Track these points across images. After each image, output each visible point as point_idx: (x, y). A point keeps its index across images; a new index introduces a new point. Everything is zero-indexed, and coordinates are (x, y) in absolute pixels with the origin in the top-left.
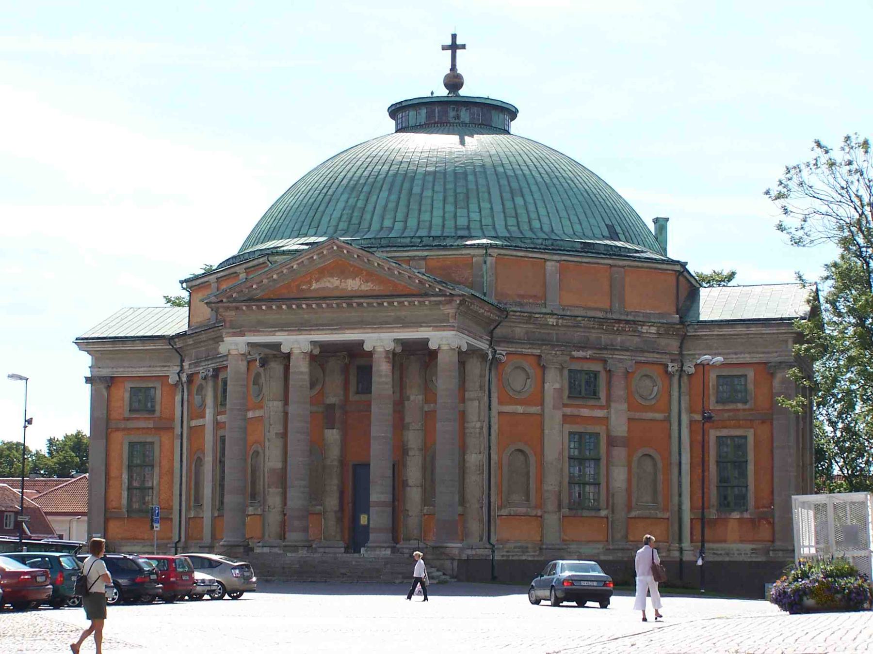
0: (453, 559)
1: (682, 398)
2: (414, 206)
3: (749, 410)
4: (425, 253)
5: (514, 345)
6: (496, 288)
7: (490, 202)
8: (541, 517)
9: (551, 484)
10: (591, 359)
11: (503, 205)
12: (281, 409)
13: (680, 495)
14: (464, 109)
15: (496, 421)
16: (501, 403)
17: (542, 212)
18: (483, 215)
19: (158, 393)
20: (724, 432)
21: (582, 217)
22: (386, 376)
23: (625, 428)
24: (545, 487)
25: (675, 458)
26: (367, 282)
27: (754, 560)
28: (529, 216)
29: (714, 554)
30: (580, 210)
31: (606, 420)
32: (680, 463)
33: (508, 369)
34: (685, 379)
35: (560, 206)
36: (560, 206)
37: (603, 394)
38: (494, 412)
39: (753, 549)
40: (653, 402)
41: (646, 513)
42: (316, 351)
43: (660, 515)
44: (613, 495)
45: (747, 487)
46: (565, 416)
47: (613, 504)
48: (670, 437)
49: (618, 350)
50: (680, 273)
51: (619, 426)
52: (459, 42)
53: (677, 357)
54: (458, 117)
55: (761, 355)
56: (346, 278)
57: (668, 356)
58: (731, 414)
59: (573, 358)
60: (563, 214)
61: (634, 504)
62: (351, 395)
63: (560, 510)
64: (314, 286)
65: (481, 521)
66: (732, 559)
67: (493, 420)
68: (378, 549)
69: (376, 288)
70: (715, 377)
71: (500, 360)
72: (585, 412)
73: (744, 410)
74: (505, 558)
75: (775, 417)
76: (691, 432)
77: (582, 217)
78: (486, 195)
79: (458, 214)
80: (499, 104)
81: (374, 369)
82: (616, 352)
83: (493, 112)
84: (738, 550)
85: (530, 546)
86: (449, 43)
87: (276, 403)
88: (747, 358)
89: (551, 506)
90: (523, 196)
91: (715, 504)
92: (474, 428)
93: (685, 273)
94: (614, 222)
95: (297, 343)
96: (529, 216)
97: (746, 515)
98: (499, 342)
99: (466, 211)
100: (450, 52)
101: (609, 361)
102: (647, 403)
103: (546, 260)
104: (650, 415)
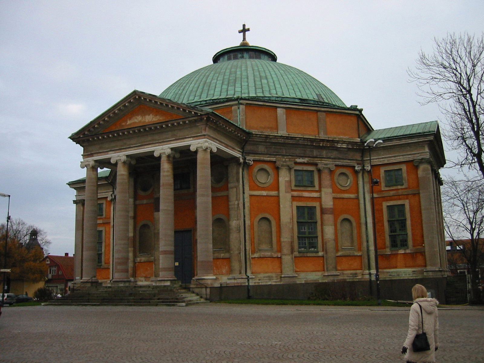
0: (206, 287)
1: (365, 185)
2: (206, 88)
7: (248, 82)
8: (280, 258)
9: (286, 237)
13: (367, 241)
15: (248, 200)
16: (251, 189)
17: (278, 86)
18: (243, 88)
19: (104, 206)
21: (302, 89)
22: (168, 171)
23: (332, 203)
24: (282, 240)
25: (363, 220)
26: (156, 115)
30: (300, 86)
31: (319, 199)
33: (256, 169)
36: (289, 84)
38: (247, 195)
39: (413, 271)
40: (348, 188)
41: (347, 253)
43: (356, 254)
44: (326, 243)
45: (407, 234)
46: (293, 197)
47: (326, 248)
48: (359, 208)
51: (328, 201)
52: (246, 28)
56: (145, 115)
59: (296, 163)
61: (339, 248)
67: (246, 200)
69: (161, 119)
71: (249, 164)
72: (306, 194)
75: (421, 191)
77: (302, 89)
78: (246, 80)
79: (229, 89)
80: (264, 50)
81: (161, 168)
84: (404, 272)
88: (401, 159)
89: (286, 250)
90: (267, 79)
91: (389, 245)
93: (361, 116)
94: (321, 93)
95: (118, 156)
98: (248, 153)
99: (233, 87)
100: (242, 33)
101: (319, 164)
102: (343, 188)
103: (277, 107)
104: (346, 196)
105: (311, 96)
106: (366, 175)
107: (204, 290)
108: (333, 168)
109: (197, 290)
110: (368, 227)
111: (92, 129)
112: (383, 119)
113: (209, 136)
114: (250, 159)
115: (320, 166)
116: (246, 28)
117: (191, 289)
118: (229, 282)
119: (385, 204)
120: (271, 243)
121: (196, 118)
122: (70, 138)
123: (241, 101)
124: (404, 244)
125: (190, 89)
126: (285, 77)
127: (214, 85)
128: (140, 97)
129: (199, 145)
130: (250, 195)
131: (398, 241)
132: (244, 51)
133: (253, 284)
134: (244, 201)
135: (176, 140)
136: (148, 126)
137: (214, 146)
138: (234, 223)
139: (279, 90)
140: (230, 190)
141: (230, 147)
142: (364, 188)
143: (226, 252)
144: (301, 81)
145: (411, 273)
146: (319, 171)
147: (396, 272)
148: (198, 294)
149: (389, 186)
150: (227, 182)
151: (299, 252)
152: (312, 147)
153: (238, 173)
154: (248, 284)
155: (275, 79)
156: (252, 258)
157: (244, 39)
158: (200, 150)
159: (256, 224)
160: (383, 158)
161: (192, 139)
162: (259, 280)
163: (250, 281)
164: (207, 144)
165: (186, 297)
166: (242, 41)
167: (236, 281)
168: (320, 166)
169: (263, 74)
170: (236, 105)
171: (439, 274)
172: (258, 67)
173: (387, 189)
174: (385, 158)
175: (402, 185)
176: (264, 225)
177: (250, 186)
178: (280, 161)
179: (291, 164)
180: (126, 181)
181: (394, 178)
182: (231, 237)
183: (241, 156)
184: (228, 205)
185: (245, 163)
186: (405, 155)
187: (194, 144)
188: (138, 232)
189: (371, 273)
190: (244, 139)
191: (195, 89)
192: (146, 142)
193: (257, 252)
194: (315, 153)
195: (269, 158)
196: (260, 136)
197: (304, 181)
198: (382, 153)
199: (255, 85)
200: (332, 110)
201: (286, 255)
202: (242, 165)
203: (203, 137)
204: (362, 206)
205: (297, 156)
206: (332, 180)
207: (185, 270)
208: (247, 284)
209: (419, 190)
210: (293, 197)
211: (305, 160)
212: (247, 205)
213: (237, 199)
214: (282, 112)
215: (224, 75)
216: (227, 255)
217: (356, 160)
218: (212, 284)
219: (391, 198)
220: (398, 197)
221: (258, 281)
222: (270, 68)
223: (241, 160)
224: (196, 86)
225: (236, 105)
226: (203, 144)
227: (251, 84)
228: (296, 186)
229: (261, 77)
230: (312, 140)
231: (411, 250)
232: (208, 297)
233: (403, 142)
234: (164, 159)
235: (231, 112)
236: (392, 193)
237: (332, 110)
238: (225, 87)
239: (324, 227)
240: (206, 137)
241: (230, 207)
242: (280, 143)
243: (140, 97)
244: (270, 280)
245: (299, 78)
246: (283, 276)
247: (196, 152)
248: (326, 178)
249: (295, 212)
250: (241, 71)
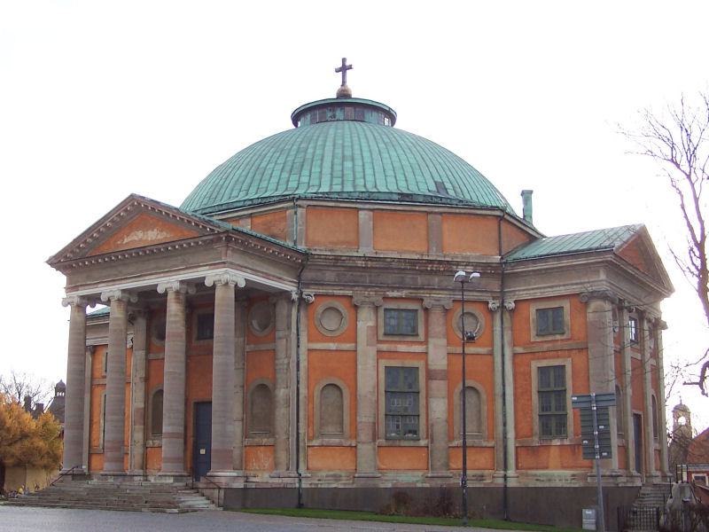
1: (505, 333)
2: (258, 177)
4: (250, 212)
5: (325, 287)
9: (365, 416)
12: (144, 357)
13: (505, 424)
14: (339, 109)
16: (309, 341)
17: (369, 171)
20: (544, 363)
22: (176, 315)
25: (498, 390)
26: (162, 231)
29: (537, 480)
30: (408, 169)
32: (504, 394)
33: (320, 309)
34: (507, 316)
35: (389, 167)
36: (389, 167)
37: (421, 331)
38: (303, 349)
39: (573, 475)
43: (484, 444)
44: (432, 425)
46: (379, 352)
49: (434, 289)
51: (439, 355)
52: (348, 64)
55: (575, 287)
57: (489, 295)
58: (550, 345)
59: (386, 298)
63: (374, 440)
64: (126, 241)
66: (552, 485)
68: (164, 478)
72: (402, 348)
73: (562, 340)
74: (313, 486)
75: (589, 345)
77: (410, 176)
82: (434, 292)
83: (366, 111)
85: (343, 474)
86: (340, 65)
87: (141, 352)
88: (562, 291)
89: (364, 435)
92: (283, 364)
93: (506, 216)
97: (566, 442)
98: (308, 285)
103: (358, 210)
106: (507, 316)
108: (449, 305)
109: (207, 492)
110: (507, 402)
111: (89, 240)
112: (562, 219)
113: (231, 263)
114: (309, 293)
115: (426, 303)
116: (348, 64)
118: (271, 481)
119: (535, 365)
120: (341, 423)
121: (211, 237)
122: (47, 262)
123: (299, 202)
126: (385, 155)
129: (217, 278)
130: (308, 350)
131: (552, 422)
132: (344, 107)
134: (298, 358)
135: (187, 268)
136: (149, 248)
137: (240, 278)
138: (281, 393)
139: (370, 178)
143: (270, 437)
146: (426, 310)
149: (543, 336)
150: (274, 329)
152: (415, 272)
153: (289, 316)
155: (367, 160)
156: (308, 446)
158: (219, 285)
159: (317, 393)
160: (533, 289)
162: (319, 480)
163: (303, 481)
164: (227, 276)
165: (184, 501)
167: (280, 481)
168: (426, 303)
169: (348, 153)
173: (539, 340)
174: (537, 288)
175: (563, 334)
176: (333, 395)
178: (359, 295)
179: (378, 299)
181: (551, 320)
182: (277, 413)
183: (295, 289)
184: (275, 365)
185: (301, 299)
186: (567, 285)
187: (210, 275)
188: (150, 401)
189: (508, 475)
190: (299, 264)
191: (242, 179)
193: (318, 438)
194: (420, 280)
195: (341, 292)
197: (401, 327)
198: (533, 281)
201: (364, 443)
203: (223, 265)
206: (447, 323)
207: (197, 465)
208: (297, 485)
210: (379, 352)
211: (404, 293)
212: (303, 364)
213: (288, 357)
214: (367, 217)
215: (288, 155)
216: (271, 441)
217: (492, 292)
219: (544, 355)
220: (556, 352)
223: (295, 296)
224: (244, 173)
228: (385, 334)
229: (343, 157)
230: (413, 262)
231: (571, 441)
232: (221, 502)
233: (565, 263)
234: (171, 297)
236: (546, 346)
238: (285, 175)
239: (431, 400)
240: (226, 265)
242: (359, 267)
244: (336, 480)
245: (410, 155)
246: (356, 475)
247: (214, 287)
248: (437, 320)
250: (315, 148)
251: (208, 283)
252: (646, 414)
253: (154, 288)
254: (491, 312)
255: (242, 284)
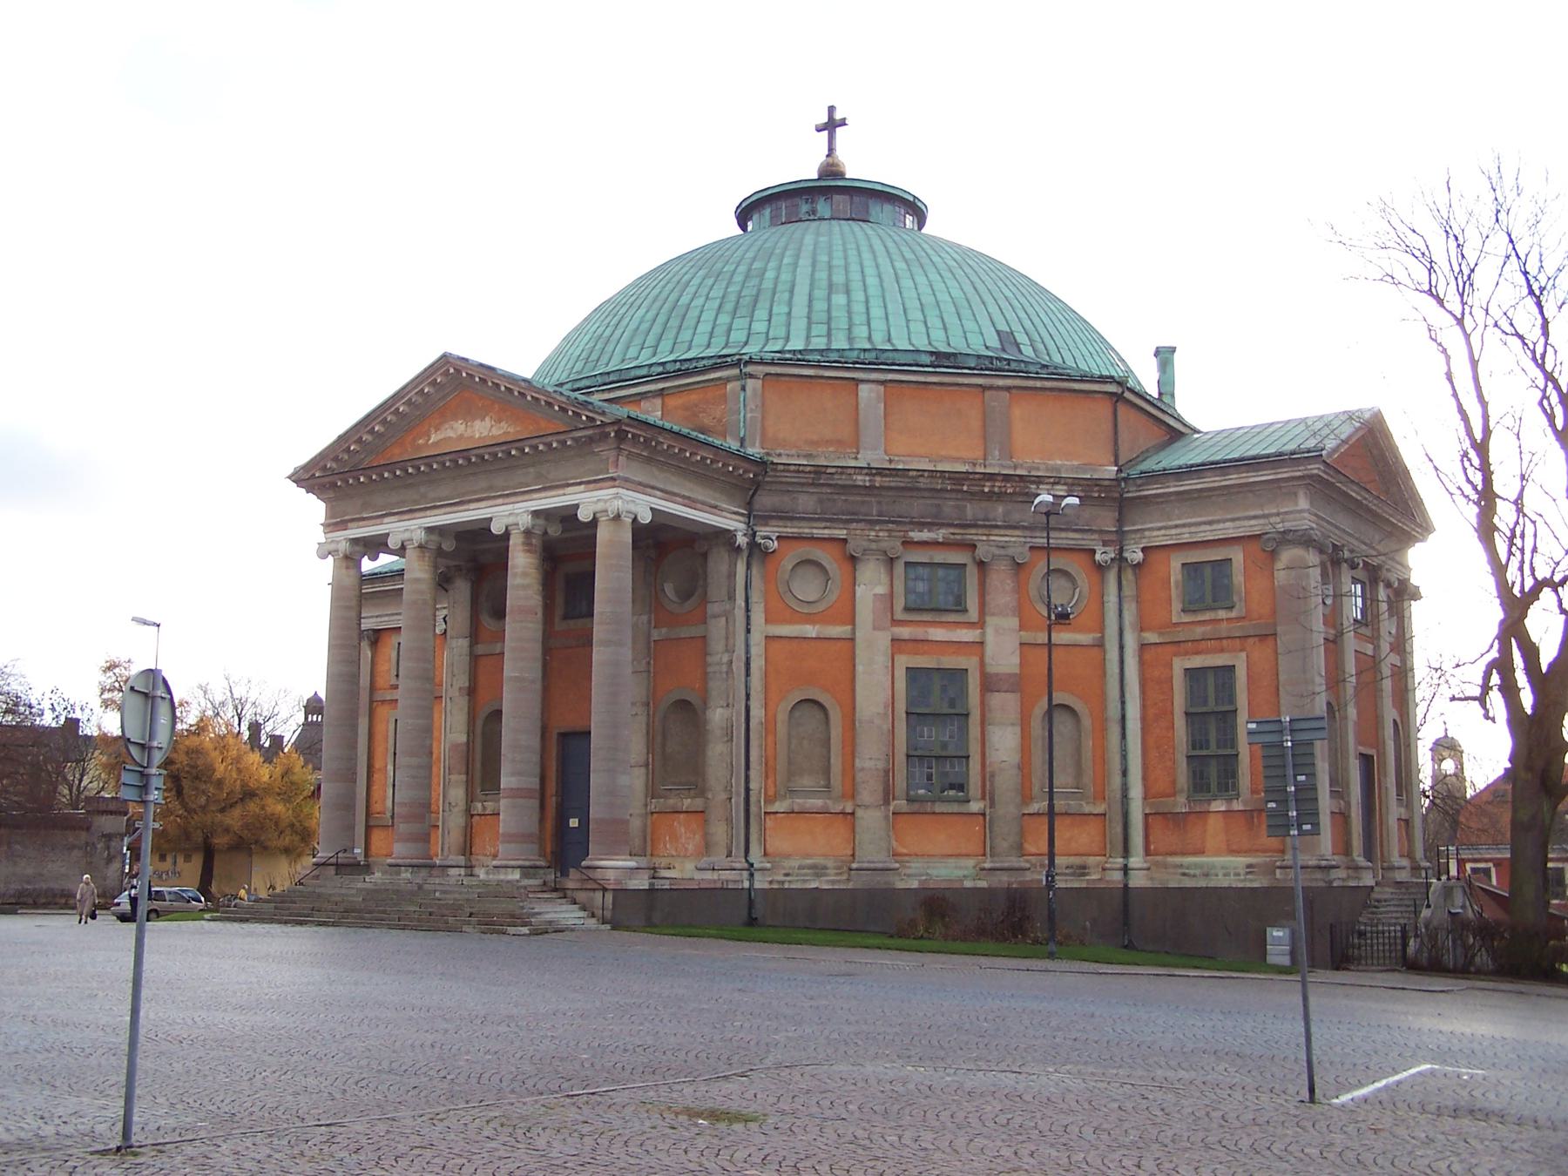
0: (605, 890)
1: (1125, 606)
3: (1239, 619)
4: (660, 386)
5: (796, 523)
6: (763, 428)
8: (853, 814)
9: (870, 758)
10: (945, 545)
11: (810, 306)
12: (466, 650)
13: (1125, 773)
17: (876, 312)
20: (1197, 662)
22: (525, 574)
23: (1016, 660)
24: (858, 763)
27: (1248, 885)
28: (850, 318)
30: (949, 309)
32: (1123, 717)
33: (788, 564)
35: (913, 304)
36: (913, 304)
38: (757, 637)
39: (1249, 866)
42: (449, 546)
43: (1087, 809)
44: (993, 775)
49: (997, 527)
50: (1117, 398)
53: (1113, 537)
54: (814, 212)
57: (1096, 536)
59: (908, 543)
60: (916, 314)
62: (557, 620)
63: (886, 802)
65: (729, 821)
66: (1212, 884)
67: (753, 651)
70: (1179, 566)
72: (938, 634)
76: (1142, 663)
77: (951, 320)
78: (786, 295)
80: (879, 188)
82: (996, 531)
83: (871, 202)
89: (869, 792)
90: (848, 292)
91: (164, 745)
92: (720, 664)
93: (1127, 395)
94: (1016, 327)
95: (408, 528)
96: (850, 318)
97: (1237, 806)
98: (765, 519)
101: (979, 545)
105: (978, 339)
106: (1129, 575)
107: (599, 895)
108: (1023, 555)
109: (581, 896)
112: (1220, 403)
113: (626, 480)
114: (768, 534)
115: (981, 552)
116: (838, 116)
117: (569, 893)
118: (698, 876)
119: (1179, 665)
120: (827, 771)
123: (749, 369)
124: (1228, 784)
125: (633, 326)
126: (907, 283)
127: (696, 313)
128: (458, 371)
133: (766, 886)
134: (747, 652)
137: (642, 506)
138: (717, 716)
140: (712, 622)
141: (703, 503)
142: (1121, 611)
144: (956, 293)
145: (1242, 872)
146: (981, 565)
147: (1200, 866)
148: (584, 909)
150: (704, 600)
151: (910, 800)
153: (732, 575)
154: (751, 884)
155: (873, 291)
157: (831, 150)
159: (782, 716)
160: (1176, 526)
161: (582, 487)
162: (787, 875)
163: (757, 876)
164: (618, 504)
166: (824, 158)
168: (981, 552)
169: (839, 278)
170: (736, 378)
171: (1318, 875)
172: (830, 255)
173: (1186, 618)
174: (1184, 526)
175: (1231, 608)
176: (811, 719)
177: (766, 611)
178: (859, 537)
180: (428, 597)
181: (1209, 584)
182: (710, 753)
184: (705, 665)
185: (753, 545)
186: (1238, 519)
187: (588, 501)
188: (479, 730)
190: (751, 480)
191: (645, 326)
192: (475, 492)
194: (971, 510)
196: (799, 469)
197: (938, 596)
199: (810, 312)
200: (1030, 383)
201: (867, 807)
202: (745, 554)
204: (1113, 667)
205: (911, 523)
206: (1020, 589)
208: (746, 885)
209: (1275, 625)
211: (940, 535)
212: (757, 664)
213: (730, 650)
214: (873, 395)
216: (698, 803)
217: (1101, 532)
218: (618, 882)
219: (1196, 646)
220: (1218, 642)
221: (781, 878)
222: (866, 255)
223: (741, 540)
225: (736, 378)
226: (615, 502)
227: (800, 309)
228: (907, 609)
229: (831, 286)
231: (1245, 803)
232: (608, 914)
233: (1234, 479)
234: (516, 541)
235: (724, 398)
236: (1199, 631)
237: (1030, 383)
238: (724, 319)
241: (710, 669)
243: (458, 371)
244: (818, 875)
246: (854, 866)
247: (594, 522)
249: (901, 685)
251: (584, 515)
252: (1382, 754)
253: (484, 525)
254: (1100, 568)
255: (646, 518)
